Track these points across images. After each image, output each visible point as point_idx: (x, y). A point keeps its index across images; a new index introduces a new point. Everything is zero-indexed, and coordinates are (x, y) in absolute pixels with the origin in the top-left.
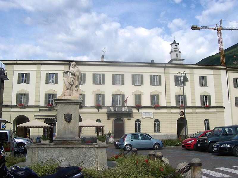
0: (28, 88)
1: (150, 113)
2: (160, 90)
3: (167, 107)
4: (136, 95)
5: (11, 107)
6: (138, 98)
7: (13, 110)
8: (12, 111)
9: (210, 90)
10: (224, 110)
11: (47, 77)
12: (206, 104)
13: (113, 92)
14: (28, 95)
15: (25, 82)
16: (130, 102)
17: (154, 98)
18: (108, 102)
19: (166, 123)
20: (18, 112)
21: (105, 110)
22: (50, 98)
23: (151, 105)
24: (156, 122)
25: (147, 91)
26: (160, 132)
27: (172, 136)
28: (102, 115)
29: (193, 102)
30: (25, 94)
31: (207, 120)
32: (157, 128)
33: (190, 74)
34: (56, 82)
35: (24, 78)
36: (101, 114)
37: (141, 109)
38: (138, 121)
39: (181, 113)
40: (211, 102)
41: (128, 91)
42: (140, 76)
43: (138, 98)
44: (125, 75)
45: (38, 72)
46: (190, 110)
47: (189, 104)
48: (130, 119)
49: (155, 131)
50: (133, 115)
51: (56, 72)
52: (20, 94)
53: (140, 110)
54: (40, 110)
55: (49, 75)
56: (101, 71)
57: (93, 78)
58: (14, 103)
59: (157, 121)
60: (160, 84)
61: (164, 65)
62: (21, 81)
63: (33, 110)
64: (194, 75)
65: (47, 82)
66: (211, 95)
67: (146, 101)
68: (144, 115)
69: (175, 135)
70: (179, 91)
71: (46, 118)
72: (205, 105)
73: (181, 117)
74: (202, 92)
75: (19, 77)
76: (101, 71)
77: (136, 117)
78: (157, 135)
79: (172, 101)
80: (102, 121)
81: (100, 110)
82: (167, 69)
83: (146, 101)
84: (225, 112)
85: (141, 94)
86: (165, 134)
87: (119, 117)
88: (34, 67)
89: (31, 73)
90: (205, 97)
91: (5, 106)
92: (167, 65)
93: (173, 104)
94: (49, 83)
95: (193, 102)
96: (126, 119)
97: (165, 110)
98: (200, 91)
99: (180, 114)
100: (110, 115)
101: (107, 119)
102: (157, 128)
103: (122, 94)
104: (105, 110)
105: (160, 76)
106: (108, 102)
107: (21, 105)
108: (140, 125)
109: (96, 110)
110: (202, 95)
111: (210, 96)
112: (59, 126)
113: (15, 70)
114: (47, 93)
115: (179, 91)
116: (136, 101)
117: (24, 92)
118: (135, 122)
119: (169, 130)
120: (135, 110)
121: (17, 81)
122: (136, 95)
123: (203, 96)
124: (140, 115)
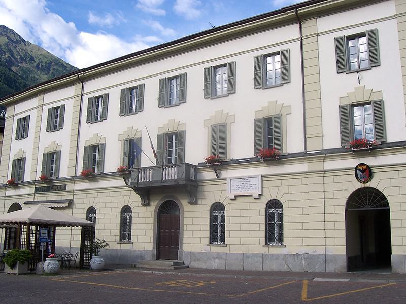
1: (253, 181)
2: (286, 98)
7: (330, 165)
8: (75, 189)
11: (206, 79)
14: (183, 133)
16: (196, 151)
17: (268, 132)
19: (306, 211)
23: (342, 142)
25: (245, 107)
27: (326, 259)
30: (176, 134)
31: (274, 204)
32: (274, 229)
33: (395, 17)
37: (226, 169)
38: (218, 207)
39: (359, 173)
41: (194, 119)
43: (219, 135)
48: (196, 203)
50: (206, 188)
51: (105, 92)
52: (266, 119)
53: (225, 174)
54: (37, 190)
55: (266, 61)
56: (59, 101)
59: (274, 204)
61: (292, 13)
62: (94, 117)
65: (343, 65)
68: (235, 188)
69: (335, 258)
70: (356, 88)
73: (359, 186)
76: (59, 101)
77: (212, 194)
78: (272, 255)
83: (242, 145)
85: (284, 113)
86: (302, 250)
87: (169, 194)
92: (301, 11)
93: (333, 140)
94: (266, 87)
96: (184, 203)
98: (337, 88)
99: (357, 177)
102: (274, 229)
103: (374, 98)
114: (261, 116)
115: (356, 88)
116: (213, 147)
120: (209, 175)
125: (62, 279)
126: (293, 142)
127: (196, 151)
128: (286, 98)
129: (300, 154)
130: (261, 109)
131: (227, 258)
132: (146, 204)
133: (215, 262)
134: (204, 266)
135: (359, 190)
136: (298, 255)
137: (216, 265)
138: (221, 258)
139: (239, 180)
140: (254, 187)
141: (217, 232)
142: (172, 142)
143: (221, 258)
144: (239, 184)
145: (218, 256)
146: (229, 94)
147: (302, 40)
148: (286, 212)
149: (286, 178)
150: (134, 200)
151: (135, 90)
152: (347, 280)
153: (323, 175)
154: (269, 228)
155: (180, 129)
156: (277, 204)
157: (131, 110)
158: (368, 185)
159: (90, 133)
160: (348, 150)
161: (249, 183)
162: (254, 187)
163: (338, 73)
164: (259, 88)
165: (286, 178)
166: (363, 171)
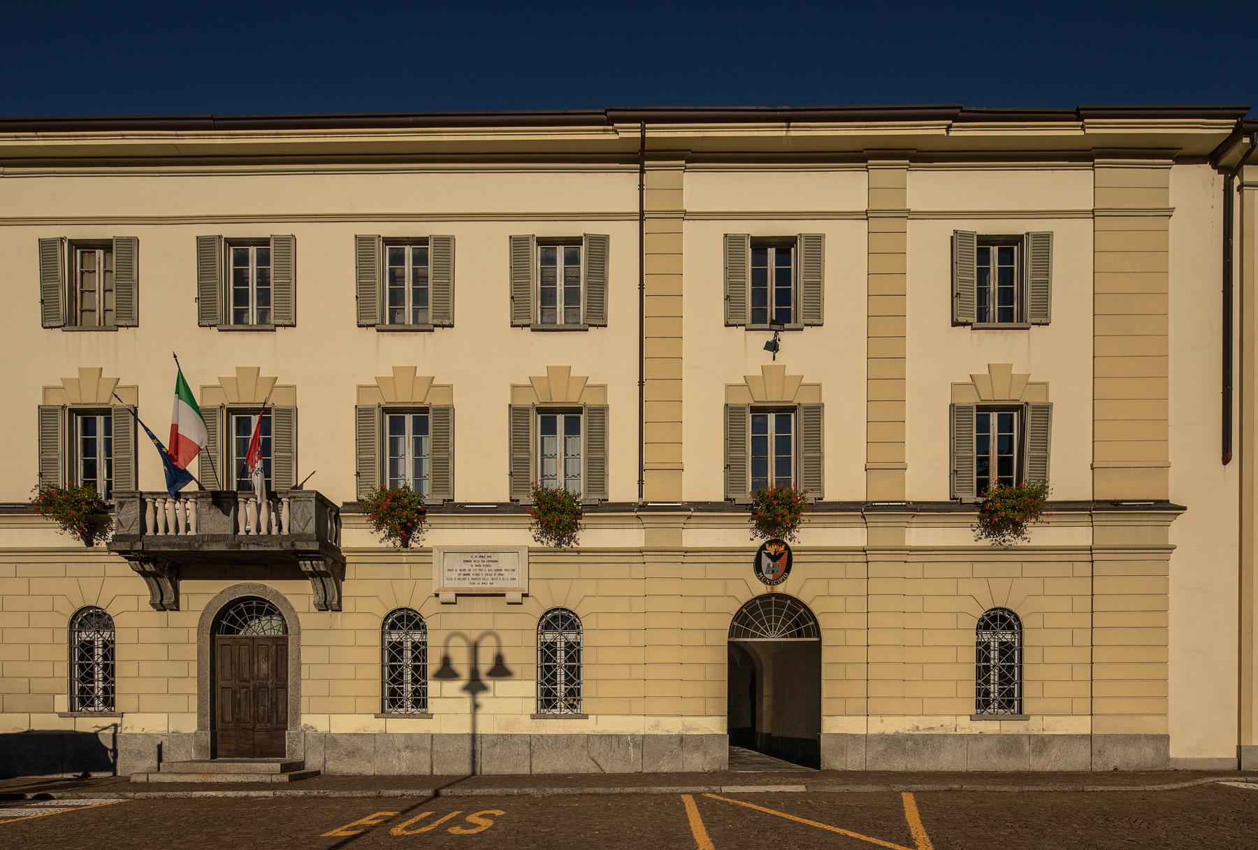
0: (822, 361)
1: (506, 561)
2: (596, 361)
3: (644, 507)
9: (1048, 360)
10: (1177, 531)
14: (446, 413)
15: (263, 316)
23: (514, 488)
24: (986, 636)
25: (482, 363)
29: (885, 463)
30: (420, 413)
32: (999, 672)
34: (124, 313)
39: (766, 561)
40: (512, 451)
45: (877, 224)
46: (853, 535)
47: (843, 478)
49: (983, 702)
57: (200, 278)
59: (560, 619)
60: (598, 318)
64: (687, 226)
73: (761, 589)
75: (731, 269)
77: (371, 590)
79: (688, 457)
80: (429, 623)
82: (658, 176)
84: (1174, 555)
93: (704, 478)
95: (885, 463)
97: (632, 536)
98: (953, 361)
108: (573, 651)
117: (417, 397)
118: (979, 627)
119: (656, 698)
121: (195, 307)
123: (759, 411)
124: (418, 571)
125: (721, 794)
126: (1068, 472)
127: (328, 461)
128: (596, 361)
129: (929, 507)
130: (218, 383)
131: (436, 748)
132: (166, 603)
133: (399, 758)
134: (369, 769)
135: (761, 597)
136: (619, 737)
137: (404, 764)
138: (419, 748)
139: (468, 557)
140: (507, 575)
141: (404, 680)
142: (258, 429)
143: (419, 748)
144: (467, 566)
145: (412, 743)
146: (435, 326)
147: (642, 213)
148: (588, 640)
149: (932, 558)
150: (121, 588)
151: (100, 253)
152: (802, 788)
153: (863, 558)
154: (393, 676)
155: (278, 401)
156: (410, 619)
157: (240, 317)
158: (780, 589)
159: (230, 362)
160: (524, 509)
161: (494, 566)
162: (507, 575)
163: (360, 326)
164: (368, 326)
165: (932, 558)
166: (775, 558)
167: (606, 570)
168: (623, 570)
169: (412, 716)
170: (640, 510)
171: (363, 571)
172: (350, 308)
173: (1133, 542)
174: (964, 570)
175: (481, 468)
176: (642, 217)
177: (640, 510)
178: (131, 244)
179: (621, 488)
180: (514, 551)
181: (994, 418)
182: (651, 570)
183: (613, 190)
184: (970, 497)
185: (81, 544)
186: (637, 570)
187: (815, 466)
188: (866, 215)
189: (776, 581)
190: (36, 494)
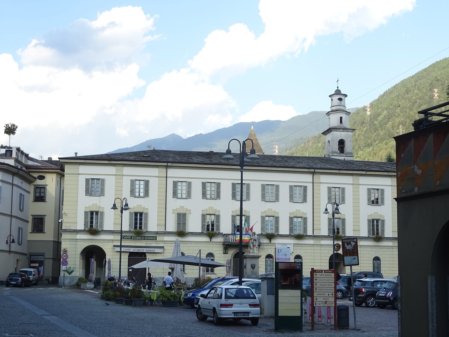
3: (314, 236)
4: (179, 215)
5: (76, 231)
6: (182, 218)
7: (79, 236)
12: (91, 226)
13: (290, 213)
18: (226, 227)
20: (86, 240)
21: (220, 239)
22: (373, 225)
23: (290, 232)
24: (267, 259)
26: (214, 274)
28: (216, 248)
30: (97, 213)
31: (377, 259)
35: (94, 187)
36: (215, 245)
39: (336, 247)
40: (306, 227)
42: (380, 191)
43: (182, 218)
44: (222, 186)
51: (189, 180)
58: (81, 226)
60: (305, 200)
63: (111, 237)
66: (308, 217)
67: (194, 225)
71: (132, 250)
72: (375, 234)
74: (371, 215)
81: (214, 240)
83: (194, 225)
88: (111, 170)
89: (252, 184)
90: (375, 221)
91: (66, 231)
93: (325, 231)
97: (311, 242)
100: (227, 247)
101: (224, 253)
104: (220, 239)
105: (305, 188)
106: (226, 227)
107: (93, 231)
109: (206, 239)
110: (371, 218)
111: (383, 221)
112: (271, 268)
113: (125, 175)
116: (179, 224)
122: (179, 215)
123: (373, 220)
158: (338, 252)
167: (193, 245)
168: (388, 250)
169: (210, 274)
170: (314, 237)
171: (362, 249)
172: (231, 197)
173: (69, 238)
174: (370, 249)
175: (284, 229)
176: (167, 177)
177: (314, 237)
178: (103, 180)
179: (310, 233)
180: (290, 244)
181: (375, 221)
182: (315, 248)
183: (308, 178)
184: (332, 235)
185: (268, 241)
186: (313, 248)
187: (383, 231)
188: (352, 184)
189: (337, 251)
190: (176, 230)
